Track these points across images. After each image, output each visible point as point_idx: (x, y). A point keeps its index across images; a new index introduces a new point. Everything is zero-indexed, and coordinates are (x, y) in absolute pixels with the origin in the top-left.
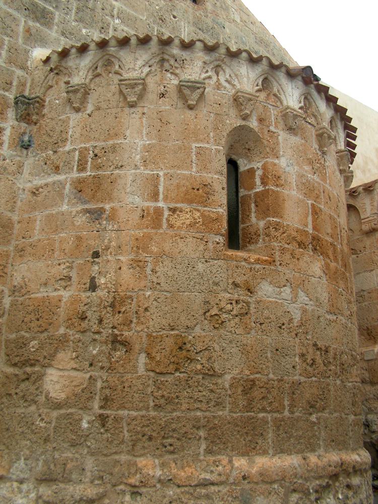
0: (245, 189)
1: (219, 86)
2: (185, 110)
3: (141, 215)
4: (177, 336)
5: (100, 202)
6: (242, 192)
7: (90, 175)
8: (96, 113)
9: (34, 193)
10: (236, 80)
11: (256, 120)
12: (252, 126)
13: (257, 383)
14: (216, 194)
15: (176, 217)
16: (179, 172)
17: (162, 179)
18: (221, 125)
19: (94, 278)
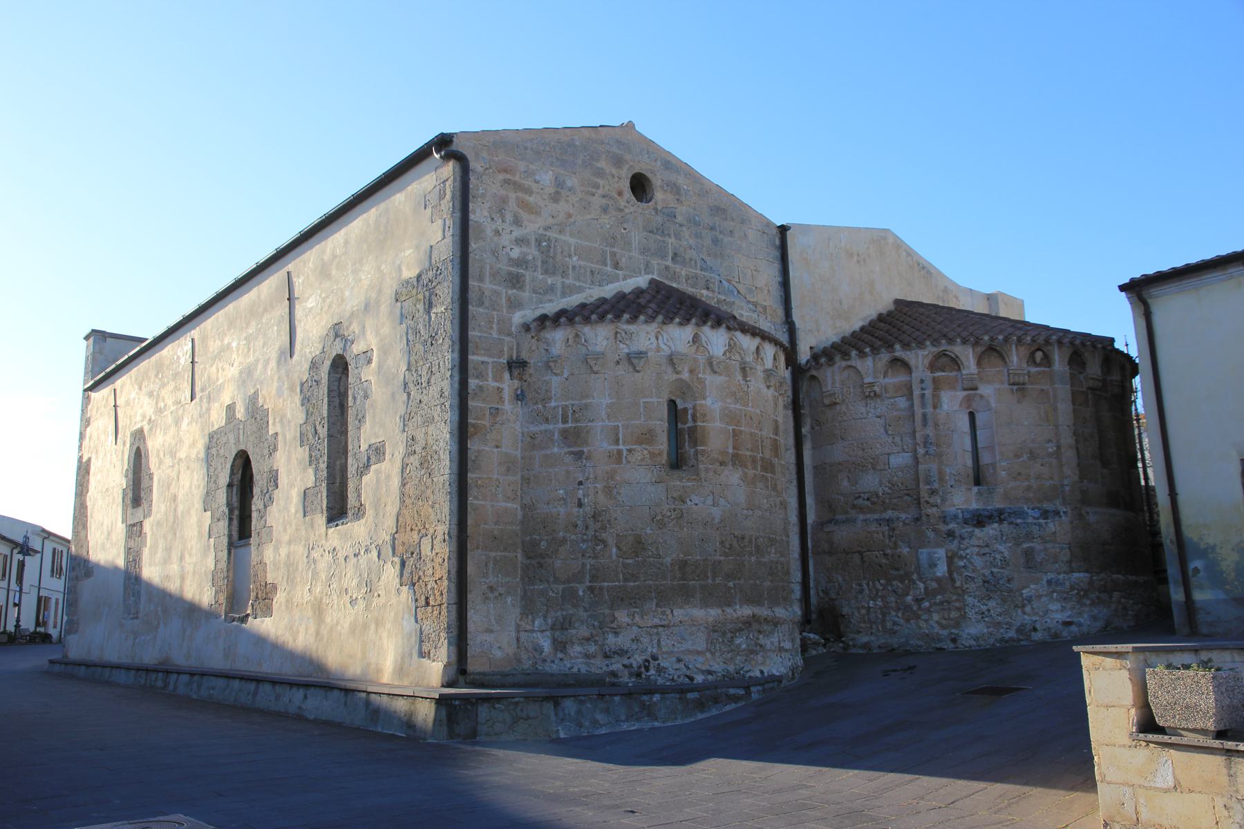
0: (682, 424)
6: (680, 426)
12: (684, 378)
13: (689, 562)
17: (621, 429)
19: (580, 499)
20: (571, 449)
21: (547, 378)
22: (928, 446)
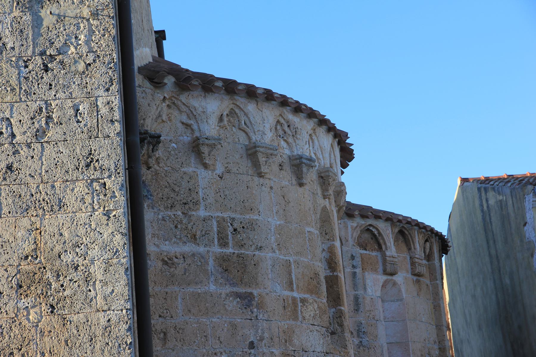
5: (248, 286)
7: (234, 253)
8: (227, 176)
9: (165, 263)
20: (235, 289)
21: (190, 170)
22: (362, 336)
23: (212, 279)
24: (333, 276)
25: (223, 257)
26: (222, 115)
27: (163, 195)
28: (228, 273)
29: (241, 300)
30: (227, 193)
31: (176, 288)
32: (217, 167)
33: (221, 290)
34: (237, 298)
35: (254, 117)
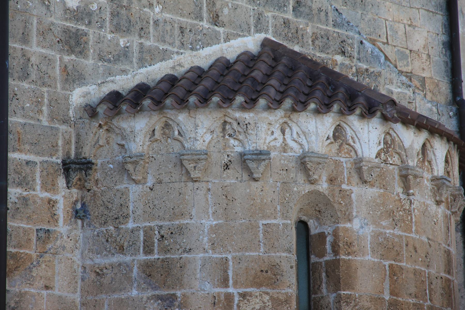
1: (286, 148)
2: (250, 183)
3: (213, 302)
4: (150, 252)
5: (171, 288)
6: (313, 259)
7: (159, 259)
8: (157, 187)
9: (98, 274)
10: (304, 138)
11: (326, 182)
14: (284, 274)
15: (246, 302)
16: (247, 254)
17: (231, 263)
18: (288, 195)
21: (121, 187)
23: (135, 285)
24: (336, 259)
25: (147, 263)
26: (154, 130)
27: (98, 213)
28: (151, 278)
29: (162, 302)
30: (156, 202)
31: (104, 296)
32: (148, 180)
33: (143, 295)
34: (158, 300)
35: (185, 126)
